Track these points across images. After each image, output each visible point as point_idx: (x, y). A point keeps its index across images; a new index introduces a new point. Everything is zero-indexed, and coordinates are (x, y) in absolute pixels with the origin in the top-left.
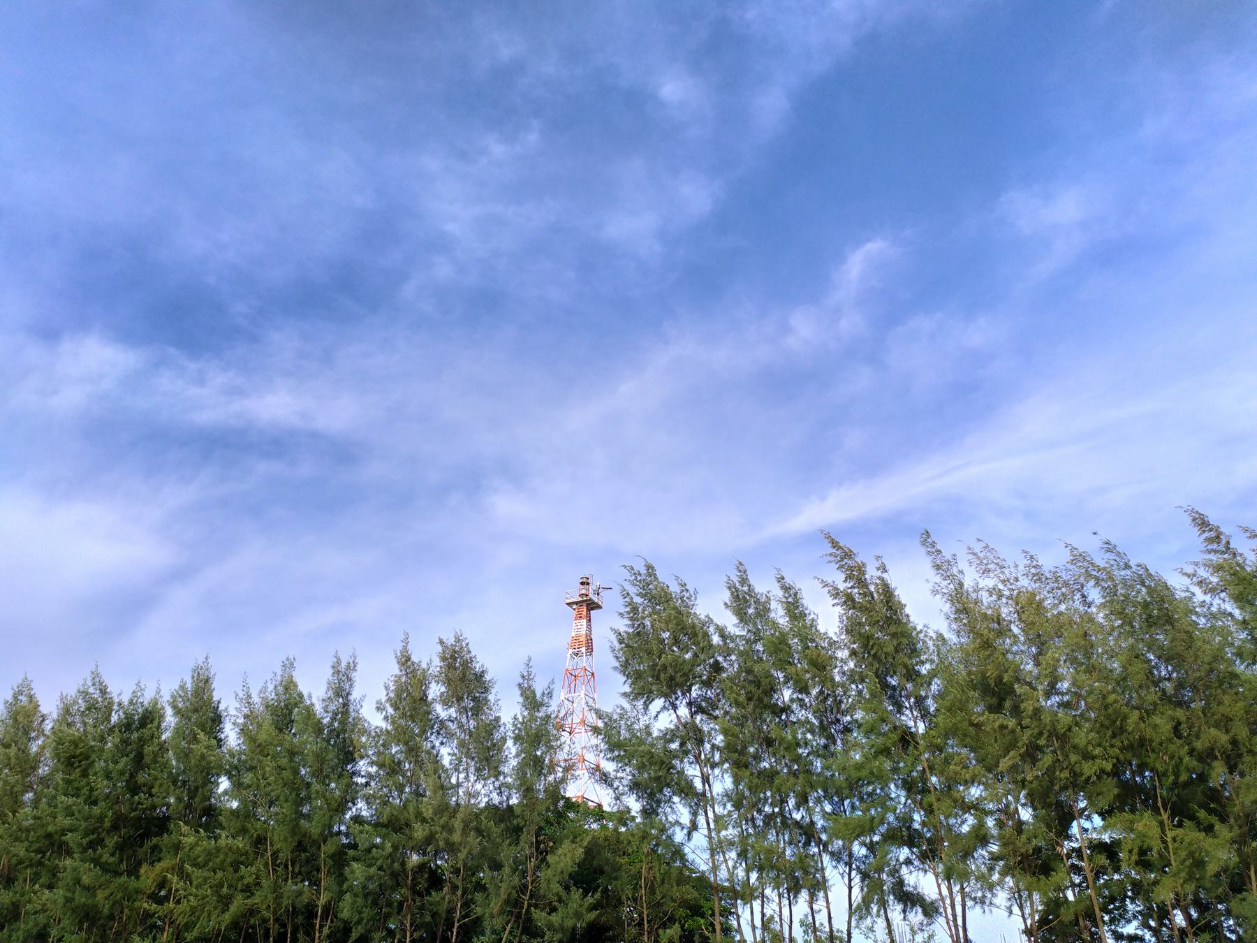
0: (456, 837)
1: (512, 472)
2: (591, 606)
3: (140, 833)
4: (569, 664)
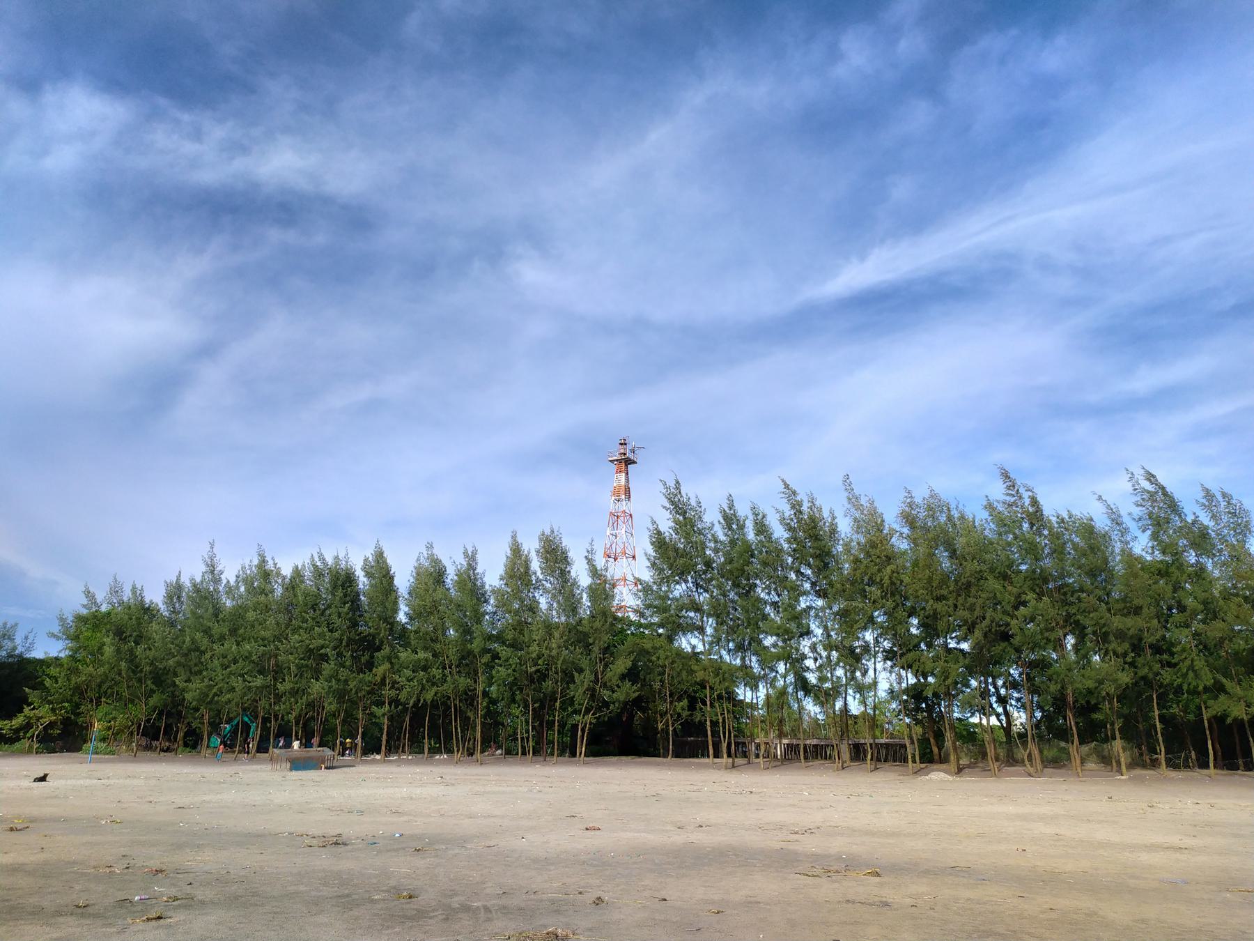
0: (554, 653)
1: (535, 235)
2: (628, 462)
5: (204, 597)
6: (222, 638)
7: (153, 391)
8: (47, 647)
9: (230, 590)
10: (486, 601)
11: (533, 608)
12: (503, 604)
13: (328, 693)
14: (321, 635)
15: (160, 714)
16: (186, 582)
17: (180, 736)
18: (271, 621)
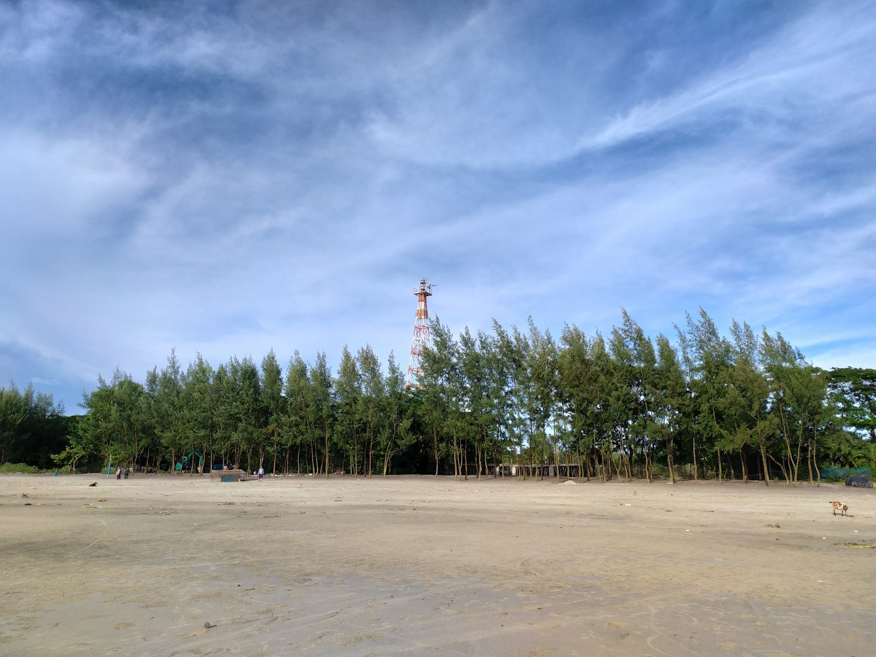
0: (370, 419)
1: (384, 103)
3: (262, 415)
4: (416, 323)
5: (169, 382)
6: (181, 407)
7: (119, 221)
8: (73, 408)
9: (183, 378)
10: (331, 386)
11: (357, 391)
12: (342, 389)
13: (242, 439)
14: (237, 407)
15: (146, 450)
16: (159, 373)
17: (158, 463)
18: (208, 399)
